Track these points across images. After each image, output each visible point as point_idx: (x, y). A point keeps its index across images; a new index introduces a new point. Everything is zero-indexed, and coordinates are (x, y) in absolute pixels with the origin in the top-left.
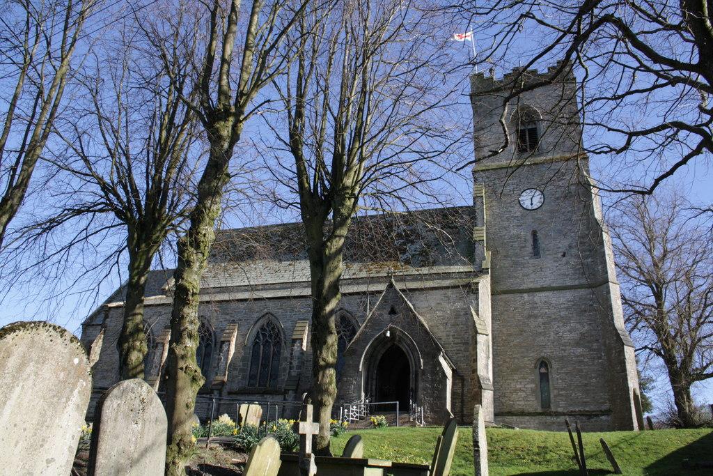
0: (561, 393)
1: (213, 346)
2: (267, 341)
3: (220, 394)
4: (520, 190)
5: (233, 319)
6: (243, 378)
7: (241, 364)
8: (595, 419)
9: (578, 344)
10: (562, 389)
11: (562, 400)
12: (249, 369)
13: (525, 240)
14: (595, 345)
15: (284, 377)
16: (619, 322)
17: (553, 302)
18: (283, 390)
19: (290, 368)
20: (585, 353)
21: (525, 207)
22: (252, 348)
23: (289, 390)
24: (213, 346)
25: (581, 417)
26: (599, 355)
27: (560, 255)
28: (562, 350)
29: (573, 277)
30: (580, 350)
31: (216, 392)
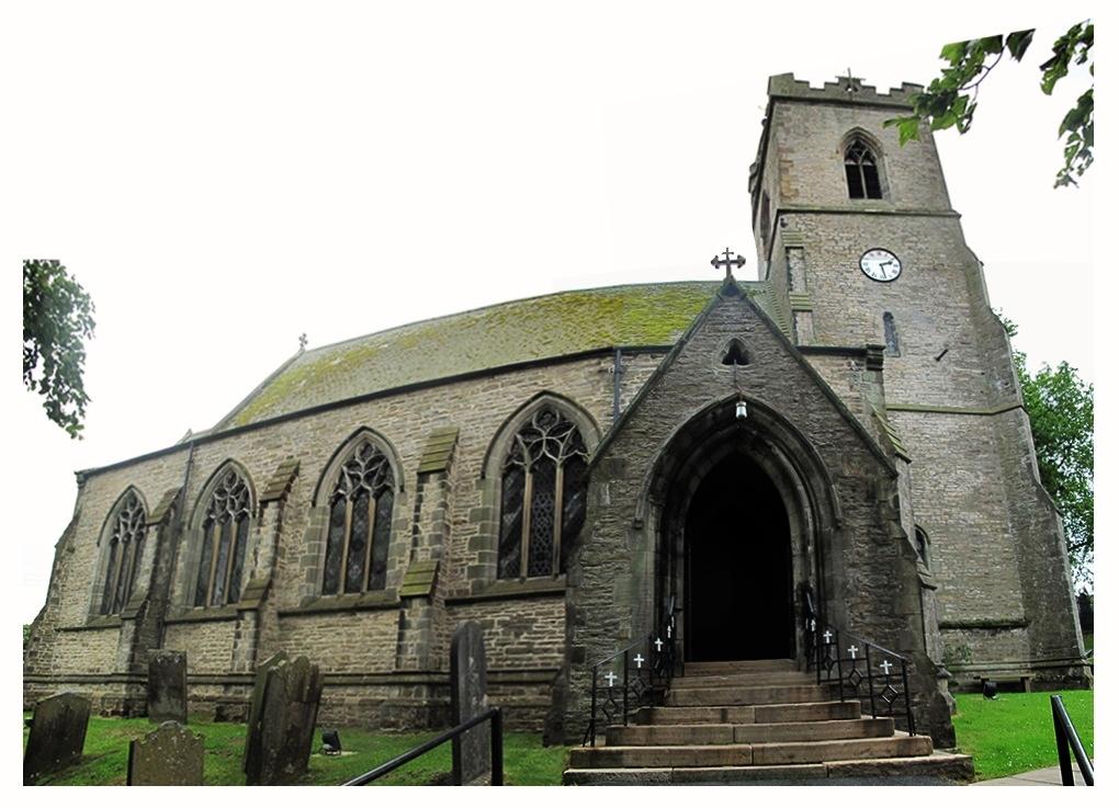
0: (946, 588)
1: (251, 516)
2: (362, 490)
3: (258, 623)
4: (861, 250)
5: (290, 454)
6: (312, 577)
7: (305, 547)
8: (1003, 633)
9: (971, 508)
10: (949, 582)
11: (950, 602)
12: (323, 554)
13: (874, 326)
14: (997, 510)
15: (398, 566)
16: (795, 599)
17: (928, 431)
18: (398, 599)
19: (415, 543)
20: (982, 522)
21: (870, 274)
22: (329, 511)
23: (411, 598)
24: (251, 516)
25: (981, 632)
26: (1004, 526)
27: (931, 358)
28: (946, 514)
29: (955, 395)
30: (974, 517)
31: (248, 616)
